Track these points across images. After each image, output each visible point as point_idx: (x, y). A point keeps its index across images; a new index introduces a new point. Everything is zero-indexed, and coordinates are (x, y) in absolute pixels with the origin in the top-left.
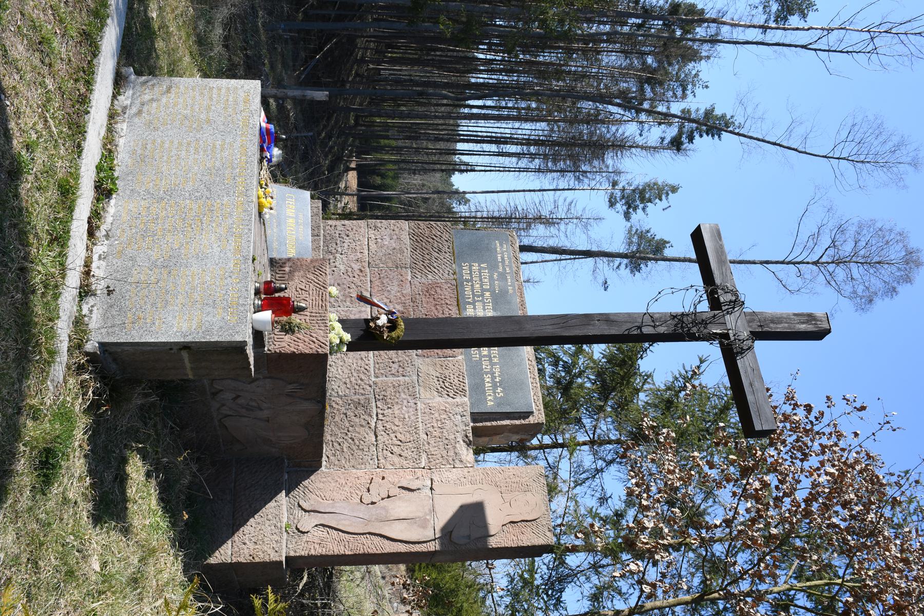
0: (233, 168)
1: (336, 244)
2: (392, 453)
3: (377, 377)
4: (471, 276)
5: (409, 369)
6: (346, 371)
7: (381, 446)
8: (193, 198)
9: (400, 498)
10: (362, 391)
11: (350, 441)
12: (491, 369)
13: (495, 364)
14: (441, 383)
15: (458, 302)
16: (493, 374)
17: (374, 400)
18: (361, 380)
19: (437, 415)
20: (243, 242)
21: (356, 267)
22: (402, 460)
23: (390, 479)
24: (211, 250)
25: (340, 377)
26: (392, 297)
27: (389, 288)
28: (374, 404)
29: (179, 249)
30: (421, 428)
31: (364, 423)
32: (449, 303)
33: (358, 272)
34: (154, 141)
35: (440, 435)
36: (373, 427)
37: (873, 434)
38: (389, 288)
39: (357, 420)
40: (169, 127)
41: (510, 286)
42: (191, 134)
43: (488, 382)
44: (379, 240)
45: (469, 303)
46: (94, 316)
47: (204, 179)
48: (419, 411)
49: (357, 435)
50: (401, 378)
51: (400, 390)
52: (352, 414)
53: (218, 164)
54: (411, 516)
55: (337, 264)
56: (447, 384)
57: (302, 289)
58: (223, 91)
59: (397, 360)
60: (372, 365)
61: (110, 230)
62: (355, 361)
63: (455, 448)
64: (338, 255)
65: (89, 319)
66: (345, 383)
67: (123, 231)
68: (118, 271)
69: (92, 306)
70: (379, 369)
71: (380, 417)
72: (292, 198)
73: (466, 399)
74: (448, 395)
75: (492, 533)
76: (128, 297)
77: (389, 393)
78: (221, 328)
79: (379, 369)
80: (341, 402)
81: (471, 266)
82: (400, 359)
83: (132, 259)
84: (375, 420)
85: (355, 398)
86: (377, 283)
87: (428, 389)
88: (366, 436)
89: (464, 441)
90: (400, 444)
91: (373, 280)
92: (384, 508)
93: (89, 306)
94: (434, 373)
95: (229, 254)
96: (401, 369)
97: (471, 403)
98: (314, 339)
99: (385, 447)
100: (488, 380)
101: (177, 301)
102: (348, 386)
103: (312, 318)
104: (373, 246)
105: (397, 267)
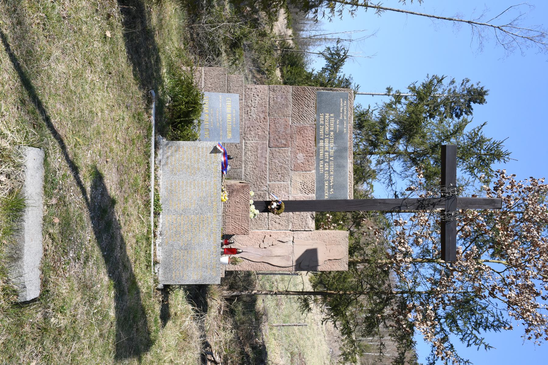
0: (211, 197)
3: (270, 182)
6: (255, 178)
7: (270, 219)
9: (278, 246)
12: (329, 178)
13: (331, 175)
16: (329, 181)
17: (268, 194)
21: (262, 116)
22: (280, 226)
28: (268, 196)
32: (310, 139)
40: (181, 172)
41: (345, 128)
42: (191, 177)
43: (326, 186)
44: (275, 99)
45: (321, 139)
46: (160, 273)
50: (282, 182)
51: (281, 189)
54: (282, 255)
55: (252, 114)
56: (305, 187)
58: (204, 149)
59: (280, 172)
60: (268, 175)
63: (306, 220)
64: (252, 108)
66: (254, 185)
67: (167, 232)
72: (229, 100)
75: (319, 264)
77: (276, 190)
81: (325, 115)
82: (283, 172)
83: (172, 245)
86: (273, 126)
87: (296, 189)
91: (271, 124)
92: (270, 250)
95: (212, 243)
96: (282, 178)
98: (243, 228)
100: (326, 184)
102: (256, 186)
104: (272, 102)
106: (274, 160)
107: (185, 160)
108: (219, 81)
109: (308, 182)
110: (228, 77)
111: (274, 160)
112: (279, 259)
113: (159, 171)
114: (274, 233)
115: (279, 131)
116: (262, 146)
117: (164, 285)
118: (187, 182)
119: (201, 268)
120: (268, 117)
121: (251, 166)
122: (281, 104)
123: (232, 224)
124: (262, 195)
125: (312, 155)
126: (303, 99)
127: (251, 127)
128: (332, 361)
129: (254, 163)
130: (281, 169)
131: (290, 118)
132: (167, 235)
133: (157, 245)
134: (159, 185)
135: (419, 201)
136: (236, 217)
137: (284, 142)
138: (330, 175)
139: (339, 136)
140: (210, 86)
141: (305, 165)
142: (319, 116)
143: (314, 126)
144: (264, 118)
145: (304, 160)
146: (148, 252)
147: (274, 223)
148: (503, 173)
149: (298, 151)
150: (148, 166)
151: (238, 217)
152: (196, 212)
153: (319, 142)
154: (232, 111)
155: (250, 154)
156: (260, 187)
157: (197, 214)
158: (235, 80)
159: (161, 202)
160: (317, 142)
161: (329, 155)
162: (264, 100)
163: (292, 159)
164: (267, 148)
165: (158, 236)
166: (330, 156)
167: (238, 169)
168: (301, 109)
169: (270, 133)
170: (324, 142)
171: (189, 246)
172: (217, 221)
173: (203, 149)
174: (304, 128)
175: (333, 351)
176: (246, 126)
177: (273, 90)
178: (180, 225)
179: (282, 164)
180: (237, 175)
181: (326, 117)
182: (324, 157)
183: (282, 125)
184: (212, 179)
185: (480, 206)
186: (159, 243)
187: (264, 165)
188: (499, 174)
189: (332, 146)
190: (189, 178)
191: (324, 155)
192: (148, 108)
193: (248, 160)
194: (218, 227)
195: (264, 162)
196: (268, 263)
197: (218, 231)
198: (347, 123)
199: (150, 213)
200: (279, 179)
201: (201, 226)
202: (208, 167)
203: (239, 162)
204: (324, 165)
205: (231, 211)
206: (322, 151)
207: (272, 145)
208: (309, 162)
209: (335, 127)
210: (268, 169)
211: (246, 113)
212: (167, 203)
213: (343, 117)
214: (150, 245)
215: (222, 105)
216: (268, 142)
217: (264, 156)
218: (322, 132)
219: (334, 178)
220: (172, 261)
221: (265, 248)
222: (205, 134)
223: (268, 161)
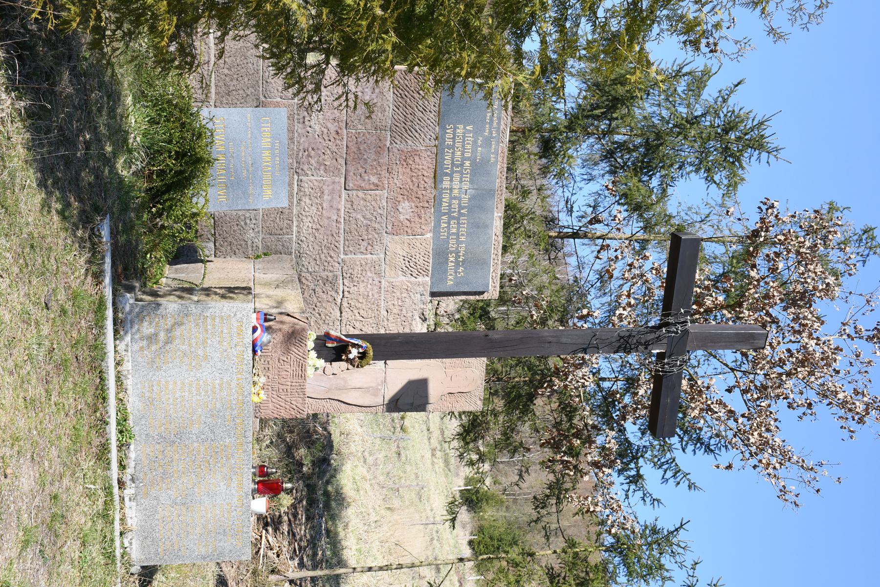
3: (346, 254)
4: (454, 142)
6: (317, 247)
7: (344, 321)
10: (331, 268)
11: (317, 315)
12: (457, 248)
13: (462, 242)
14: (407, 262)
15: (435, 174)
16: (457, 253)
17: (341, 278)
18: (331, 257)
19: (398, 294)
21: (333, 127)
25: (310, 254)
27: (365, 157)
28: (341, 281)
29: (193, 488)
30: (383, 305)
31: (331, 299)
32: (426, 174)
35: (399, 312)
36: (339, 304)
37: (851, 293)
38: (365, 157)
39: (324, 296)
41: (493, 153)
42: (192, 373)
43: (452, 262)
45: (447, 174)
46: (134, 546)
48: (383, 289)
49: (324, 310)
50: (369, 256)
51: (367, 269)
52: (320, 290)
53: (218, 405)
54: (365, 386)
55: (312, 123)
56: (411, 264)
58: (217, 320)
60: (342, 242)
62: (325, 237)
63: (411, 324)
66: (315, 260)
67: (145, 474)
69: (131, 539)
71: (346, 293)
73: (428, 279)
74: (412, 275)
75: (431, 402)
77: (356, 271)
79: (348, 247)
80: (310, 278)
81: (455, 128)
82: (370, 236)
83: (157, 498)
84: (341, 296)
85: (324, 274)
87: (393, 268)
88: (332, 311)
89: (420, 318)
90: (362, 319)
91: (350, 144)
93: (129, 539)
94: (401, 252)
95: (234, 491)
96: (370, 247)
97: (432, 283)
98: (294, 407)
99: (348, 323)
100: (452, 259)
101: (196, 532)
102: (318, 263)
106: (354, 215)
108: (245, 61)
109: (418, 254)
115: (365, 159)
116: (331, 187)
120: (345, 131)
121: (310, 225)
124: (330, 279)
125: (427, 205)
126: (415, 95)
127: (310, 149)
129: (316, 220)
131: (389, 133)
133: (127, 499)
135: (623, 337)
137: (374, 179)
138: (459, 243)
139: (479, 168)
140: (226, 71)
141: (413, 225)
142: (443, 129)
143: (434, 150)
144: (337, 133)
145: (412, 214)
148: (772, 207)
149: (400, 198)
153: (442, 181)
154: (273, 144)
155: (308, 201)
156: (326, 264)
159: (131, 422)
160: (438, 180)
161: (459, 204)
163: (388, 213)
164: (340, 191)
165: (128, 483)
166: (461, 207)
167: (284, 234)
168: (409, 116)
169: (348, 162)
170: (451, 180)
172: (244, 452)
173: (214, 319)
174: (415, 153)
176: (301, 148)
178: (172, 461)
179: (369, 223)
180: (283, 246)
181: (458, 131)
182: (449, 210)
183: (372, 147)
184: (234, 376)
185: (728, 344)
187: (334, 224)
188: (766, 207)
189: (466, 187)
190: (186, 376)
191: (450, 205)
192: (98, 277)
193: (303, 213)
195: (335, 218)
196: (339, 401)
198: (498, 144)
199: (109, 464)
200: (363, 249)
202: (225, 354)
203: (286, 221)
204: (449, 223)
205: (271, 376)
206: (446, 198)
207: (351, 185)
208: (420, 218)
209: (474, 151)
210: (342, 231)
211: (301, 121)
213: (491, 132)
215: (252, 132)
216: (343, 180)
218: (448, 162)
219: (466, 247)
221: (333, 374)
222: (219, 195)
223: (342, 215)
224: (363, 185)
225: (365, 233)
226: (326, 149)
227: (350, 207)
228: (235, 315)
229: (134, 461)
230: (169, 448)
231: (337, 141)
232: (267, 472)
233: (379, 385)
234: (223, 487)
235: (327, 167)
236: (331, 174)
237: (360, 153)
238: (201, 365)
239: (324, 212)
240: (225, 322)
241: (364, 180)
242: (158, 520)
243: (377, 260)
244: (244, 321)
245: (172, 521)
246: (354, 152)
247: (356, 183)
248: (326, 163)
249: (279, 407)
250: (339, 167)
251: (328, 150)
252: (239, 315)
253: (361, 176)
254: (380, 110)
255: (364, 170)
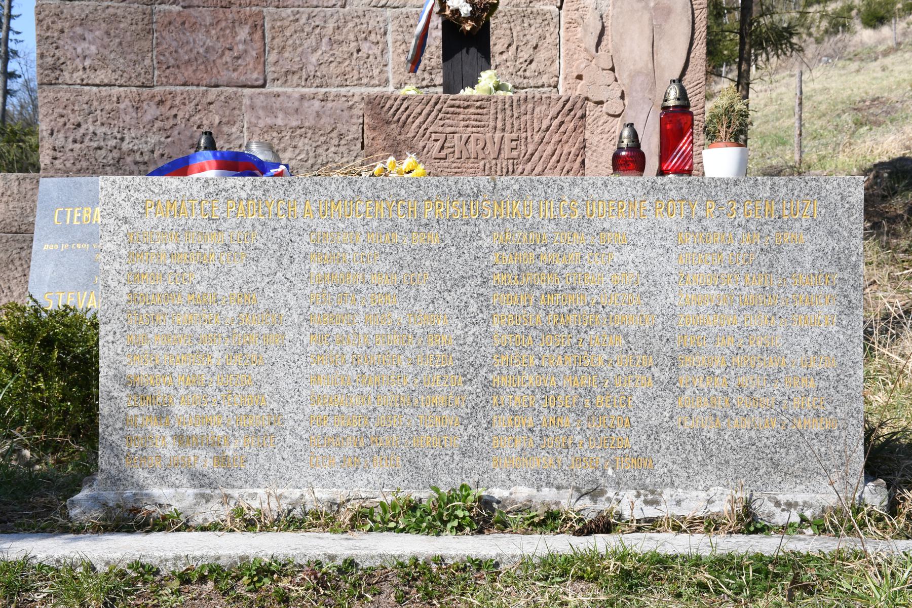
0: (396, 227)
1: (100, 148)
2: (531, 62)
3: (387, 81)
5: (372, 23)
8: (486, 315)
9: (617, 51)
20: (606, 196)
21: (152, 111)
22: (544, 45)
23: (583, 66)
24: (631, 266)
26: (219, 46)
27: (201, 50)
33: (163, 109)
34: (312, 419)
38: (201, 50)
40: (267, 389)
42: (289, 335)
44: (87, 63)
47: (426, 291)
50: (390, 38)
54: (648, 33)
55: (146, 148)
57: (442, 148)
58: (140, 267)
59: (353, 44)
61: (578, 490)
64: (125, 146)
65: (810, 506)
68: (687, 460)
69: (778, 504)
70: (372, 77)
72: (64, 213)
76: (753, 434)
78: (830, 233)
79: (372, 77)
82: (351, 37)
83: (653, 433)
86: (188, 73)
90: (514, 47)
92: (632, 77)
93: (777, 511)
95: (642, 225)
96: (373, 37)
98: (556, 122)
99: (521, 73)
101: (762, 329)
103: (508, 127)
104: (102, 76)
105: (150, 31)
106: (311, 68)
107: (199, 369)
108: (17, 263)
110: (8, 229)
111: (311, 68)
112: (661, 45)
113: (255, 505)
114: (569, 64)
115: (207, 50)
116: (261, 113)
117: (867, 480)
118: (320, 358)
119: (776, 282)
120: (157, 89)
121: (333, 149)
122: (106, 40)
123: (538, 169)
128: (851, 56)
129: (323, 139)
130: (340, 43)
132: (600, 458)
134: (332, 503)
136: (506, 153)
144: (161, 102)
146: (705, 576)
147: (533, 66)
150: (203, 579)
151: (507, 146)
152: (473, 308)
157: (485, 304)
158: (15, 204)
159: (425, 495)
162: (95, 103)
164: (267, 95)
165: (602, 505)
169: (214, 81)
171: (656, 344)
175: (826, 56)
177: (54, 68)
178: (544, 390)
179: (325, 40)
186: (639, 503)
187: (330, 105)
190: (298, 348)
193: (310, 162)
194: (553, 192)
195: (317, 104)
197: (577, 190)
199: (479, 564)
200: (376, 50)
201: (548, 282)
202: (235, 247)
207: (255, 76)
210: (343, 91)
212: (429, 463)
214: (662, 562)
216: (247, 91)
217: (297, 104)
220: (736, 435)
221: (622, 97)
223: (313, 90)
224: (254, 53)
225: (345, 48)
226: (191, 123)
227: (296, 77)
228: (125, 220)
229: (538, 489)
230: (504, 397)
231: (177, 102)
232: (629, 149)
233: (646, 7)
234: (628, 254)
235: (224, 120)
236: (237, 112)
237: (196, 60)
238: (268, 311)
239: (307, 124)
240: (145, 247)
241: (246, 51)
242: (720, 431)
243: (396, 21)
244: (141, 196)
245: (725, 393)
246: (195, 71)
247: (251, 66)
248: (217, 121)
249: (555, 158)
250: (222, 98)
251: (192, 119)
252: (127, 210)
253: (238, 58)
254: (115, 24)
255: (227, 52)
